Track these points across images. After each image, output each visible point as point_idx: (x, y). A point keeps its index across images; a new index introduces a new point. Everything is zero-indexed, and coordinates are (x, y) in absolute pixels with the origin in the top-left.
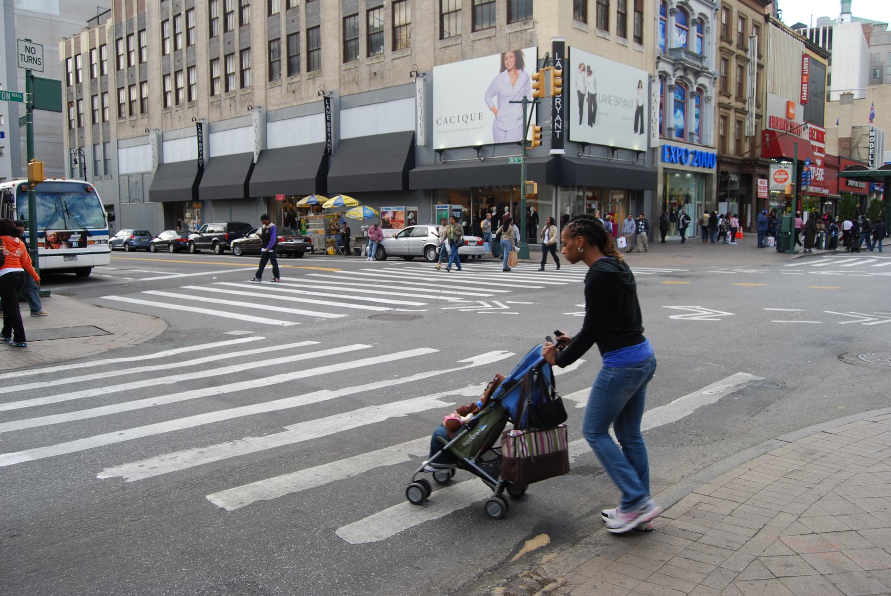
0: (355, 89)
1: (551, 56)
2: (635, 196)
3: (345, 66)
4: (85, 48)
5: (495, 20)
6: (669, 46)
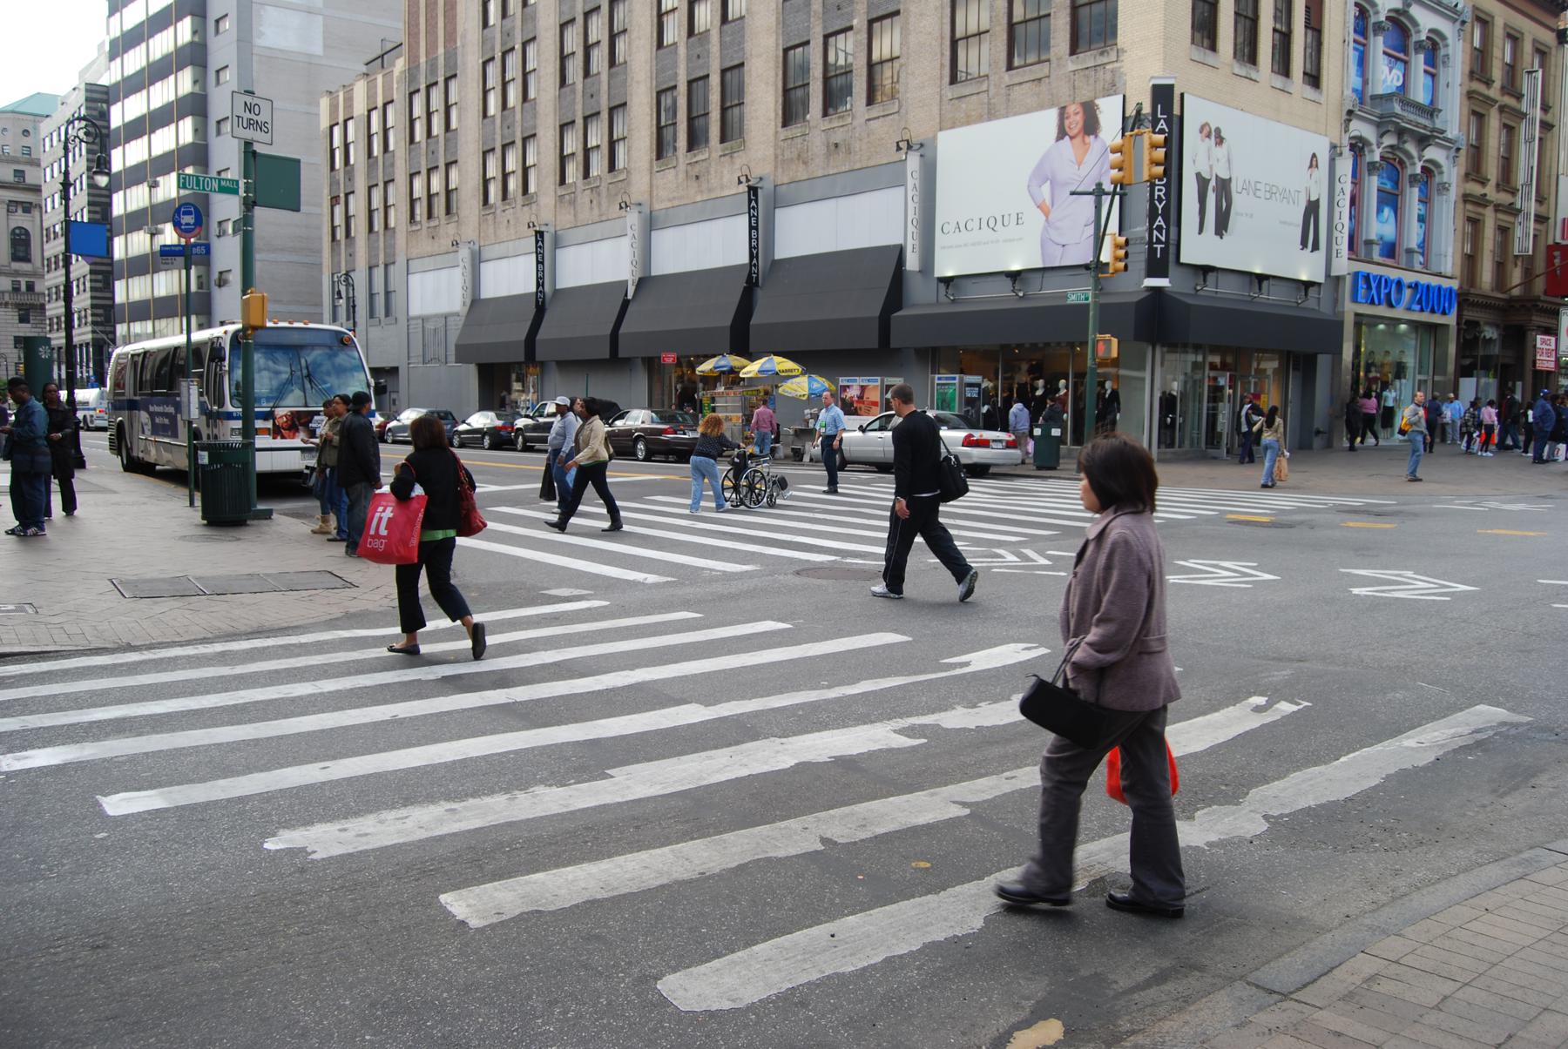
0: (802, 174)
1: (1147, 109)
2: (1300, 364)
3: (784, 133)
4: (360, 108)
5: (1048, 48)
6: (1370, 91)
